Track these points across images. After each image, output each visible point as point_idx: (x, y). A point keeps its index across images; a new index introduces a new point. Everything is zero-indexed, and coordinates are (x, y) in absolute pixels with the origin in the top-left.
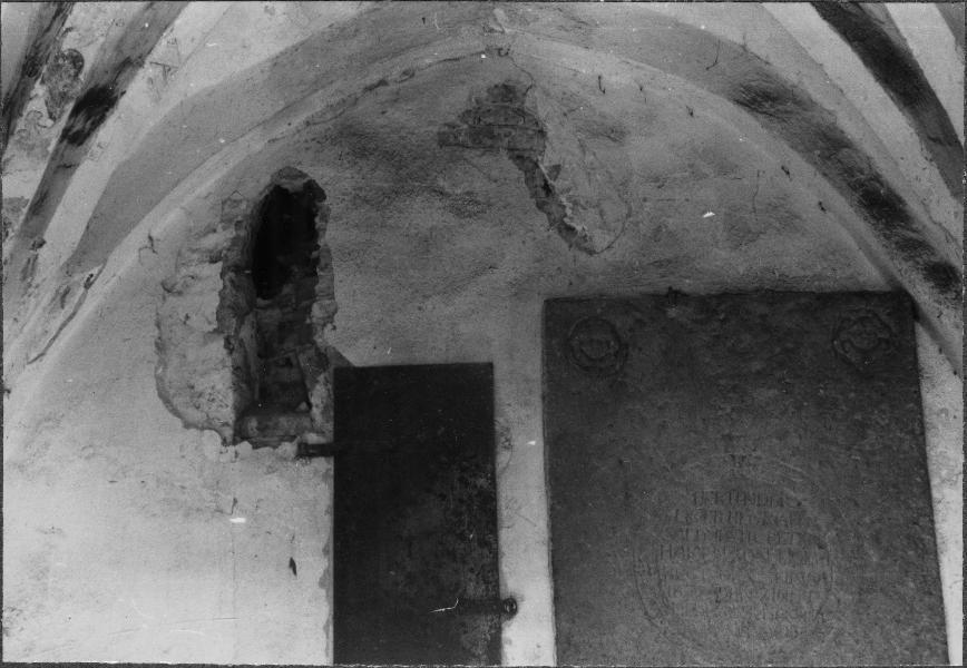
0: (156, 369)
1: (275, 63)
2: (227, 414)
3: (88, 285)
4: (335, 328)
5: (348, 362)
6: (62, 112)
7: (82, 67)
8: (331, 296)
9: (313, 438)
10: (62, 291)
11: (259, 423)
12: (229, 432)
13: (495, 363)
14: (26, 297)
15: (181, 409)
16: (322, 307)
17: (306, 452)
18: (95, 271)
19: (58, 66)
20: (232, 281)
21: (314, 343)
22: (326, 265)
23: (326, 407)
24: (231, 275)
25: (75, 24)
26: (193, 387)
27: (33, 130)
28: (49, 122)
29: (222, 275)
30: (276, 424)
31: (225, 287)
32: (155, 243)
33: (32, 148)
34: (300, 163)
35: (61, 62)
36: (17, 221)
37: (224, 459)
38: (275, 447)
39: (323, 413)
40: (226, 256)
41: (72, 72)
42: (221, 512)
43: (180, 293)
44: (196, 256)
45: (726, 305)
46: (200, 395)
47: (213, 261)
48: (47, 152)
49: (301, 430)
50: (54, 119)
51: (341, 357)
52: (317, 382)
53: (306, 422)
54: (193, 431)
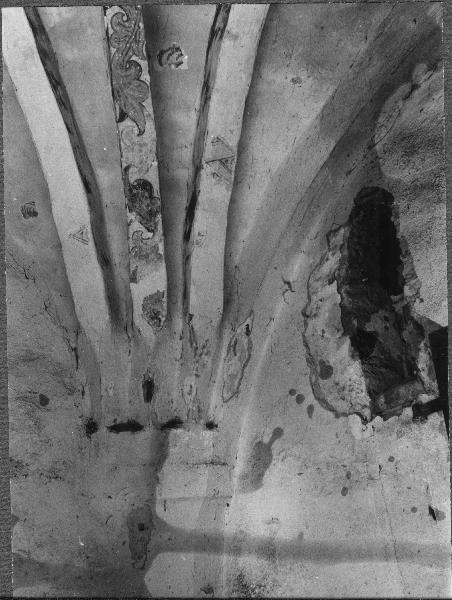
0: (310, 378)
1: (322, 117)
2: (364, 398)
3: (248, 332)
4: (422, 300)
5: (440, 326)
6: (156, 224)
7: (151, 187)
8: (414, 276)
9: (425, 398)
10: (233, 343)
11: (386, 398)
12: (367, 413)
13: (156, 383)
14: (197, 358)
15: (333, 404)
16: (411, 287)
17: (421, 413)
18: (248, 321)
19: (135, 195)
20: (347, 293)
21: (412, 318)
22: (407, 252)
23: (430, 369)
24: (346, 287)
25: (129, 162)
26: (337, 384)
27: (141, 244)
28: (150, 235)
29: (339, 291)
30: (398, 394)
31: (342, 299)
32: (292, 285)
33: (147, 256)
34: (371, 181)
35: (135, 191)
36: (163, 309)
37: (367, 434)
38: (399, 415)
39: (429, 374)
40: (339, 275)
41: (147, 194)
42: (372, 479)
43: (315, 315)
44: (320, 283)
45: (255, 69)
46: (344, 388)
47: (330, 283)
48: (161, 255)
49: (416, 395)
50: (152, 231)
51: (431, 323)
52: (419, 350)
53: (418, 386)
54: (342, 419)
